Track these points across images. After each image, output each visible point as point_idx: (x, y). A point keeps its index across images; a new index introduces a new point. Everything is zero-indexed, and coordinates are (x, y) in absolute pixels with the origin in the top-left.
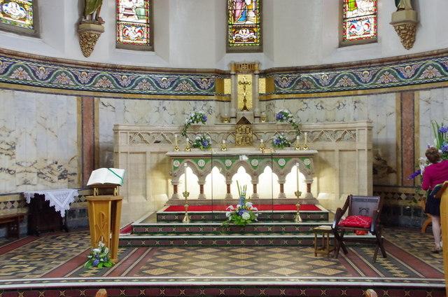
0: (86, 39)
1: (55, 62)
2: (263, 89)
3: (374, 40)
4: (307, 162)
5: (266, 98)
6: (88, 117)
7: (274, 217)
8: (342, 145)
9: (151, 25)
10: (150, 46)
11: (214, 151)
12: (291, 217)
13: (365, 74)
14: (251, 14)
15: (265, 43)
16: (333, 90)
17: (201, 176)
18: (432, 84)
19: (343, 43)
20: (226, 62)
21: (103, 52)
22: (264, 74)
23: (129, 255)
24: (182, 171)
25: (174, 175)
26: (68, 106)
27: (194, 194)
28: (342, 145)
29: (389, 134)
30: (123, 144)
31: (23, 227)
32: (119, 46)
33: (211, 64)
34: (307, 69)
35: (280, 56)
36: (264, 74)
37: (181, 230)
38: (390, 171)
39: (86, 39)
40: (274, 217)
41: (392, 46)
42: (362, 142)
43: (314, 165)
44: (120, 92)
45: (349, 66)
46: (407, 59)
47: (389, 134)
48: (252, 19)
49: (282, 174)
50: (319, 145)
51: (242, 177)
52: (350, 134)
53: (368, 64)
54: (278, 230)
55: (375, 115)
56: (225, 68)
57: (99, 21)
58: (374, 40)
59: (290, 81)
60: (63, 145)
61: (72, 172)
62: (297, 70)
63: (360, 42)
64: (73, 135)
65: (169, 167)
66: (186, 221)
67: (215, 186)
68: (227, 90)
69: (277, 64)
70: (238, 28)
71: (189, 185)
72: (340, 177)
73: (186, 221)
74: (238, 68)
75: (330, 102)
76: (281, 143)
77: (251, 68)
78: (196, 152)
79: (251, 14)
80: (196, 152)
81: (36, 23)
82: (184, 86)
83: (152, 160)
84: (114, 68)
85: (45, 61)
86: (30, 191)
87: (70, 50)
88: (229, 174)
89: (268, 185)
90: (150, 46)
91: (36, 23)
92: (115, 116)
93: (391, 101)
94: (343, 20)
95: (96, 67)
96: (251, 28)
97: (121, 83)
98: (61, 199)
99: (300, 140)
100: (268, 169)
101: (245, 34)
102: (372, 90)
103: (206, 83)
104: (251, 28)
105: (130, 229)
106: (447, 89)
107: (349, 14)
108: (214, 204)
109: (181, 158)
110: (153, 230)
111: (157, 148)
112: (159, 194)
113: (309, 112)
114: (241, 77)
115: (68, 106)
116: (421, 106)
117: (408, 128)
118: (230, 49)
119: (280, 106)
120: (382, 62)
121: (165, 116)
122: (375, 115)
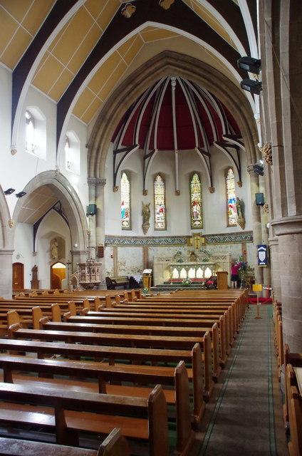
0: (145, 230)
1: (136, 237)
4: (212, 266)
5: (204, 244)
6: (146, 253)
8: (223, 261)
9: (166, 222)
10: (166, 229)
14: (199, 216)
16: (224, 242)
19: (229, 226)
20: (191, 232)
21: (150, 233)
22: (203, 236)
23: (50, 98)
24: (173, 270)
25: (171, 271)
26: (139, 250)
27: (193, 277)
28: (223, 261)
30: (156, 262)
31: (128, 286)
32: (155, 229)
34: (216, 235)
36: (203, 236)
37: (170, 286)
39: (145, 230)
41: (239, 229)
42: (228, 260)
44: (155, 245)
45: (229, 234)
48: (200, 218)
50: (217, 261)
52: (224, 258)
54: (196, 286)
55: (234, 250)
56: (191, 235)
57: (148, 224)
60: (139, 262)
61: (284, 436)
62: (213, 235)
64: (142, 258)
65: (170, 268)
66: (171, 284)
67: (183, 274)
69: (207, 234)
70: (195, 221)
71: (175, 274)
74: (194, 235)
75: (224, 246)
76: (205, 260)
77: (199, 234)
78: (179, 264)
79: (199, 216)
80: (179, 264)
81: (131, 226)
84: (154, 237)
85: (133, 237)
86: (129, 276)
87: (140, 233)
89: (192, 274)
90: (166, 229)
91: (131, 226)
92: (155, 253)
93: (240, 246)
94: (228, 218)
95: (147, 238)
96: (199, 221)
97: (155, 242)
98: (138, 278)
101: (197, 223)
102: (235, 242)
103: (185, 240)
104: (199, 221)
105: (157, 286)
107: (230, 216)
109: (172, 266)
110: (162, 286)
111: (167, 262)
112: (167, 277)
114: (196, 238)
115: (139, 250)
118: (192, 228)
120: (237, 233)
121: (169, 252)
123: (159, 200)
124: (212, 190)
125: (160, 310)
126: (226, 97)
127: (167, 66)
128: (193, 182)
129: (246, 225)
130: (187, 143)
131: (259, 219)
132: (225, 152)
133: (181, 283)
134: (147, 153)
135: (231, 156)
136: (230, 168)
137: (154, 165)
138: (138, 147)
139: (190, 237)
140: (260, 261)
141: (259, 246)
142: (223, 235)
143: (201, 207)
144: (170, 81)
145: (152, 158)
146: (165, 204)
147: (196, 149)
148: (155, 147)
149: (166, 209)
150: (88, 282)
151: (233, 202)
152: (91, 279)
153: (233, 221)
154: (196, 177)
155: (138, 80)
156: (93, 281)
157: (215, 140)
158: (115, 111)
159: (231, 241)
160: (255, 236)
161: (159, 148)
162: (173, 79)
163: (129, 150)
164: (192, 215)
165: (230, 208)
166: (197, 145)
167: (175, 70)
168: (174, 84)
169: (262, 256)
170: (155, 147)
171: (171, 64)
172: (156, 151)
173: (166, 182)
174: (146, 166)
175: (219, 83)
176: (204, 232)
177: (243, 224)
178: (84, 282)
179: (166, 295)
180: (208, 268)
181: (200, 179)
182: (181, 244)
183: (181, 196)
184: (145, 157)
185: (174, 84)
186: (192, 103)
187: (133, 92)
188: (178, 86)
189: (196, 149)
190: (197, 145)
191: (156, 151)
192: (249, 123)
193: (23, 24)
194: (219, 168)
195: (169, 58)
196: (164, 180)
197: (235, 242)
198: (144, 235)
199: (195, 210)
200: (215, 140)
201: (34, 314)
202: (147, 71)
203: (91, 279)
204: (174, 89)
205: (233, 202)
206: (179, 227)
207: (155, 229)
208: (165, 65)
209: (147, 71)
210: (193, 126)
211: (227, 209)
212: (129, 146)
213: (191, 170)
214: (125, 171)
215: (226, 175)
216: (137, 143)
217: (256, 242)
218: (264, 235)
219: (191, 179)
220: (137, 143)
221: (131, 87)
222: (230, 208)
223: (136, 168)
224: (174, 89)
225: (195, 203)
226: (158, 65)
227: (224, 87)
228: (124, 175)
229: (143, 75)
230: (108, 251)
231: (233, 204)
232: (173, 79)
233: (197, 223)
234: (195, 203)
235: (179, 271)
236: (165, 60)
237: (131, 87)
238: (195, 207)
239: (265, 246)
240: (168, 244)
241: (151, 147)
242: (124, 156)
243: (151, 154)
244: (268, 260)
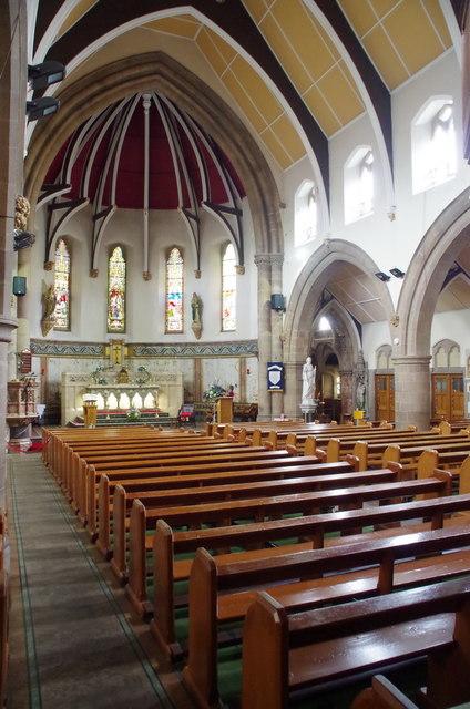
2: (126, 353)
3: (182, 332)
5: (128, 357)
7: (146, 416)
8: (170, 383)
10: (69, 329)
11: (109, 386)
12: (105, 416)
13: (179, 349)
15: (128, 328)
17: (118, 398)
18: (208, 356)
19: (167, 332)
20: (107, 338)
21: (51, 335)
27: (127, 406)
28: (170, 383)
29: (190, 378)
33: (102, 341)
34: (151, 345)
35: (137, 337)
36: (127, 345)
37: (155, 420)
38: (190, 395)
40: (146, 416)
41: (190, 337)
42: (180, 382)
43: (157, 391)
44: (58, 354)
45: (225, 343)
46: (198, 344)
47: (190, 378)
48: (121, 316)
49: (143, 396)
51: (137, 399)
53: (180, 344)
55: (181, 369)
58: (182, 332)
59: (148, 350)
62: (145, 345)
63: (175, 332)
66: (108, 418)
67: (125, 403)
68: (107, 353)
72: (169, 398)
73: (108, 418)
74: (114, 342)
77: (121, 342)
78: (101, 386)
80: (101, 386)
82: (208, 351)
83: (78, 390)
88: (131, 397)
89: (137, 401)
93: (235, 361)
99: (69, 371)
100: (137, 394)
101: (116, 324)
103: (98, 350)
106: (466, 514)
108: (148, 410)
111: (80, 384)
113: (152, 365)
114: (114, 347)
116: (204, 366)
117: (198, 376)
119: (137, 363)
120: (186, 344)
122: (181, 369)
123: (61, 283)
124: (147, 277)
125: (139, 456)
126: (237, 152)
127: (157, 77)
128: (113, 259)
129: (203, 335)
130: (164, 200)
131: (270, 330)
132: (187, 221)
133: (125, 416)
134: (99, 211)
135: (227, 224)
136: (229, 242)
137: (70, 225)
138: (87, 202)
139: (106, 345)
140: (270, 384)
141: (270, 364)
142: (162, 344)
143: (125, 297)
144: (142, 100)
145: (108, 219)
146: (69, 288)
147: (180, 210)
148: (113, 202)
149: (70, 297)
150: (22, 415)
151: (176, 297)
152: (26, 410)
153: (175, 326)
154: (175, 252)
155: (110, 82)
156: (31, 415)
157: (205, 199)
158: (66, 118)
159: (174, 355)
160: (263, 348)
161: (119, 204)
162: (147, 96)
163: (73, 205)
164: (109, 310)
165: (170, 307)
166: (181, 204)
167: (168, 88)
168: (147, 105)
169: (275, 377)
170: (113, 202)
171: (162, 75)
172: (115, 208)
173: (75, 254)
174: (51, 232)
175: (231, 129)
176: (127, 339)
177: (199, 332)
178: (16, 416)
179: (111, 433)
180: (137, 394)
181: (182, 256)
182: (94, 356)
183: (99, 275)
184: (96, 217)
185: (147, 105)
186: (174, 135)
187: (98, 99)
188: (153, 109)
189: (180, 210)
190: (181, 204)
191: (115, 208)
192: (267, 198)
193: (385, 22)
194: (210, 243)
195: (156, 63)
196: (70, 250)
197: (181, 357)
198: (41, 337)
199: (113, 304)
200: (205, 199)
201: (336, 456)
202: (126, 74)
203: (26, 410)
204: (147, 113)
205: (176, 297)
206: (90, 328)
207: (167, 332)
208: (155, 74)
209: (126, 74)
210: (94, 165)
211: (167, 306)
212: (74, 200)
213: (113, 242)
214: (65, 238)
215: (168, 257)
216: (86, 195)
217: (264, 359)
218: (276, 350)
219: (110, 255)
220: (86, 195)
221: (96, 88)
222: (170, 307)
223: (79, 236)
224: (147, 113)
225: (114, 293)
226: (145, 69)
227: (238, 138)
228: (62, 243)
229: (119, 77)
230: (36, 363)
231: (177, 301)
232: (147, 96)
233: (116, 324)
234: (114, 293)
235: (131, 397)
236: (157, 66)
237: (96, 88)
238: (114, 299)
239: (280, 364)
240: (75, 355)
241: (106, 201)
242: (68, 213)
243: (105, 213)
244: (282, 383)
